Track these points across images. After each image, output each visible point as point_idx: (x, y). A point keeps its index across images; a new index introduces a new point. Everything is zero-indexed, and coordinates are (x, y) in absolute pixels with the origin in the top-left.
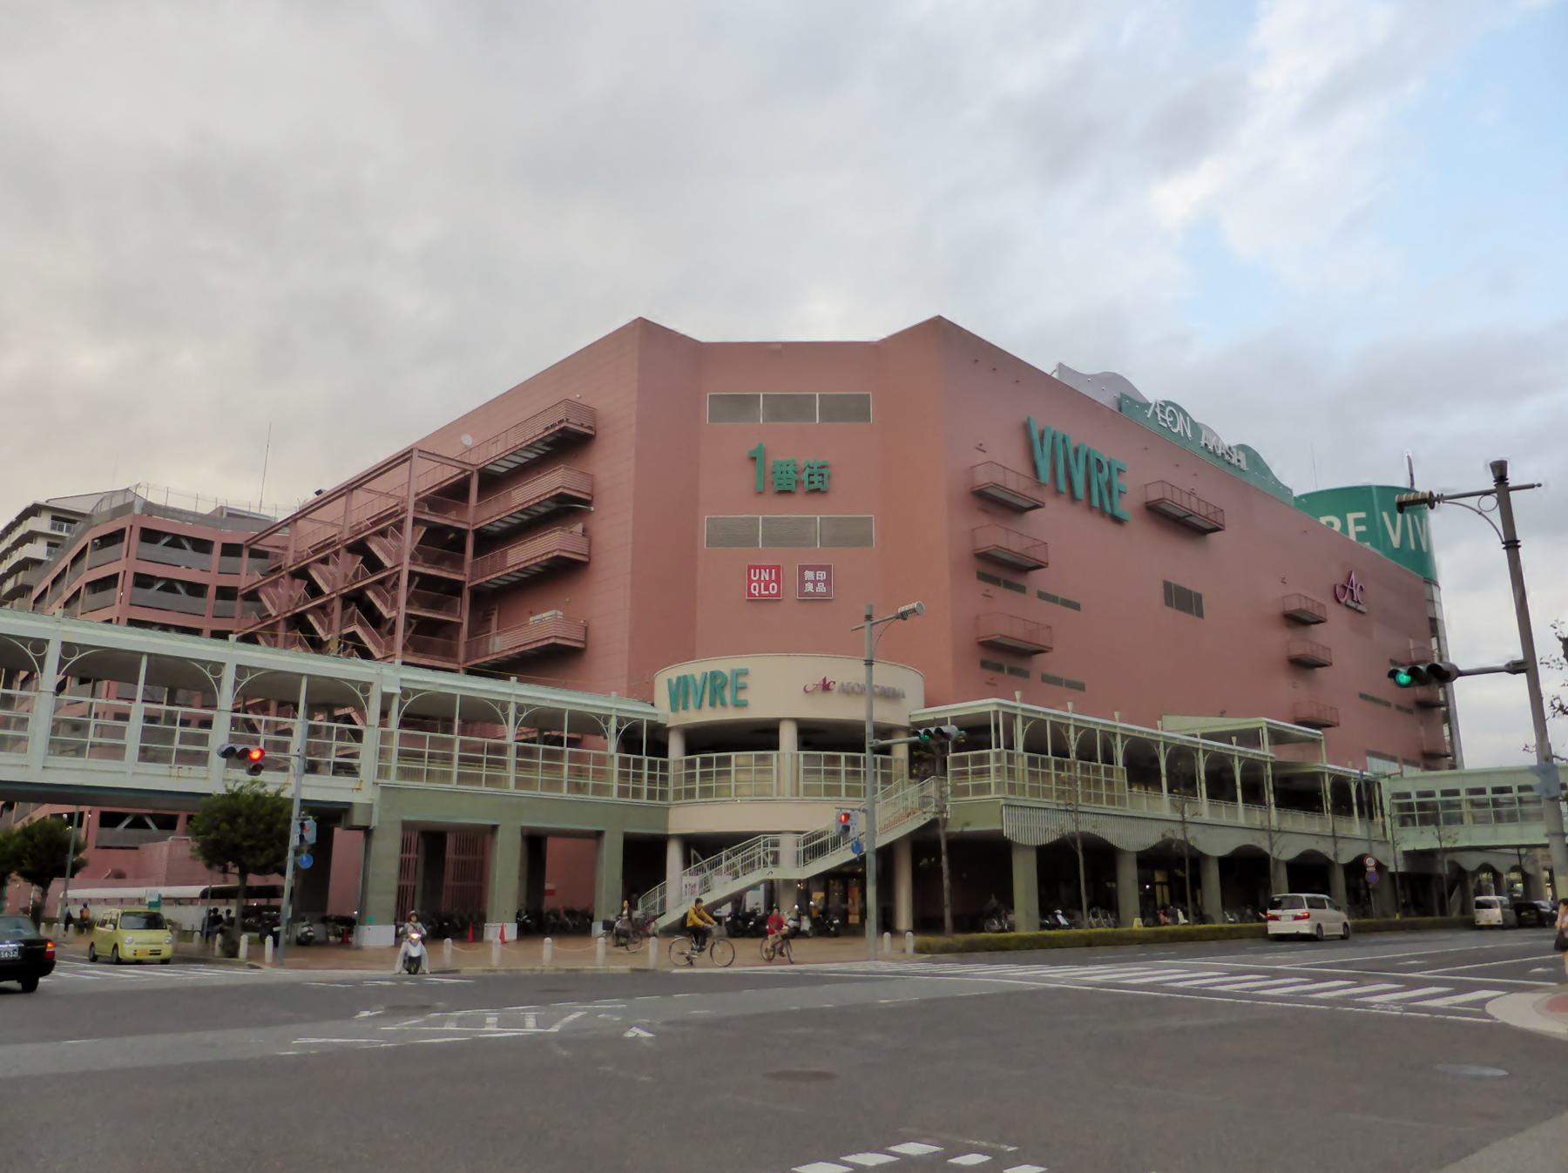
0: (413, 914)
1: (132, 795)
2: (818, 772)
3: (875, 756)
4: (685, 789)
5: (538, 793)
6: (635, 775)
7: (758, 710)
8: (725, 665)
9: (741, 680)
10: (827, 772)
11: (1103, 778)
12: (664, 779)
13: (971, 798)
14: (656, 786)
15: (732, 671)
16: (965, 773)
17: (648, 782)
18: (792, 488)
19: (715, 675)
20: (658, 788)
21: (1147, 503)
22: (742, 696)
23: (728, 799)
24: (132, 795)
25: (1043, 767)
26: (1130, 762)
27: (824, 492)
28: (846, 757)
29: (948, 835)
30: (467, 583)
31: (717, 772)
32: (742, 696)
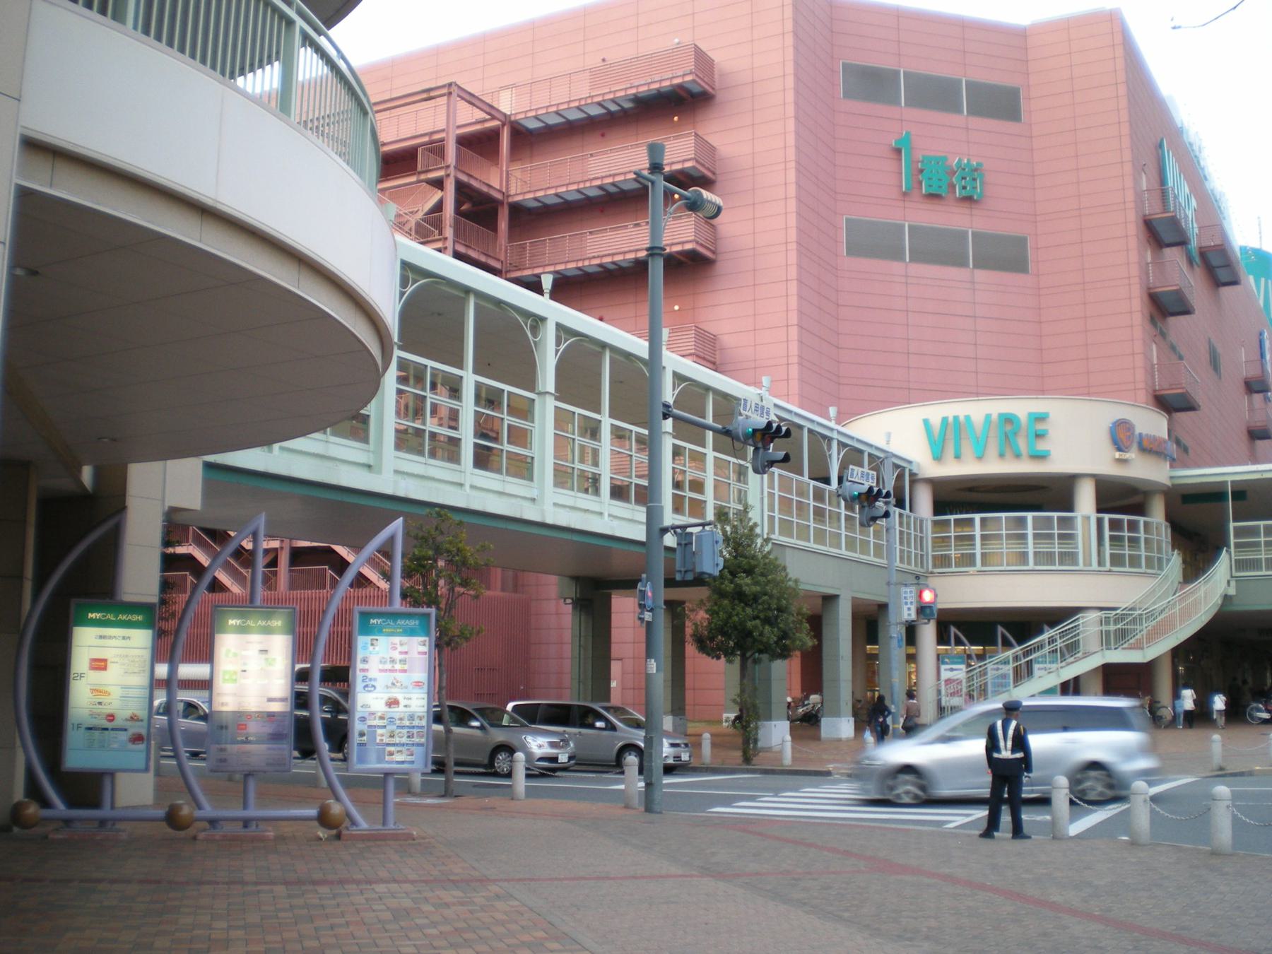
0: (877, 690)
1: (576, 538)
2: (1050, 536)
3: (1101, 515)
4: (1140, 556)
5: (930, 553)
6: (1131, 540)
7: (1059, 464)
8: (1022, 408)
9: (1041, 427)
10: (1061, 536)
11: (872, 540)
12: (1134, 542)
13: (1263, 573)
14: (1125, 550)
15: (1030, 414)
16: (1050, 536)
17: (1111, 545)
18: (943, 192)
19: (1008, 420)
20: (1127, 552)
21: (1200, 248)
22: (1042, 446)
23: (925, 557)
24: (576, 538)
25: (799, 516)
26: (823, 516)
27: (976, 202)
28: (1034, 518)
29: (635, 597)
30: (1161, 325)
31: (1059, 534)
32: (1042, 446)
